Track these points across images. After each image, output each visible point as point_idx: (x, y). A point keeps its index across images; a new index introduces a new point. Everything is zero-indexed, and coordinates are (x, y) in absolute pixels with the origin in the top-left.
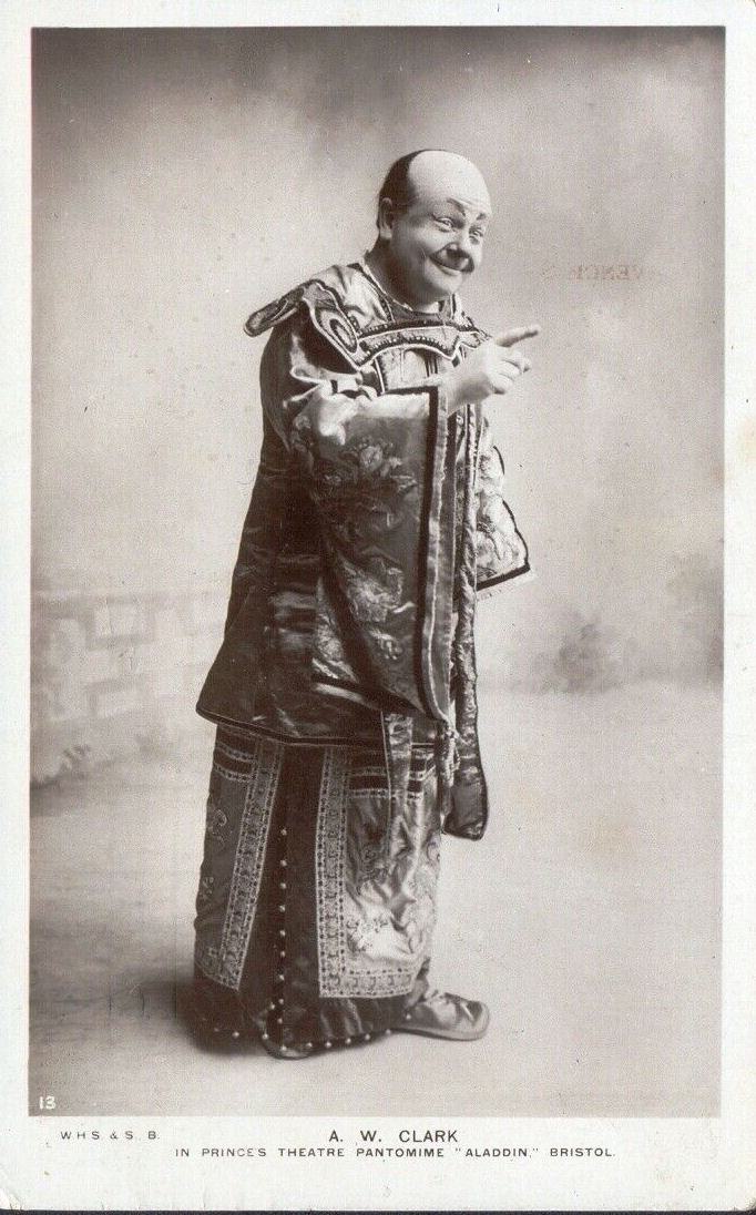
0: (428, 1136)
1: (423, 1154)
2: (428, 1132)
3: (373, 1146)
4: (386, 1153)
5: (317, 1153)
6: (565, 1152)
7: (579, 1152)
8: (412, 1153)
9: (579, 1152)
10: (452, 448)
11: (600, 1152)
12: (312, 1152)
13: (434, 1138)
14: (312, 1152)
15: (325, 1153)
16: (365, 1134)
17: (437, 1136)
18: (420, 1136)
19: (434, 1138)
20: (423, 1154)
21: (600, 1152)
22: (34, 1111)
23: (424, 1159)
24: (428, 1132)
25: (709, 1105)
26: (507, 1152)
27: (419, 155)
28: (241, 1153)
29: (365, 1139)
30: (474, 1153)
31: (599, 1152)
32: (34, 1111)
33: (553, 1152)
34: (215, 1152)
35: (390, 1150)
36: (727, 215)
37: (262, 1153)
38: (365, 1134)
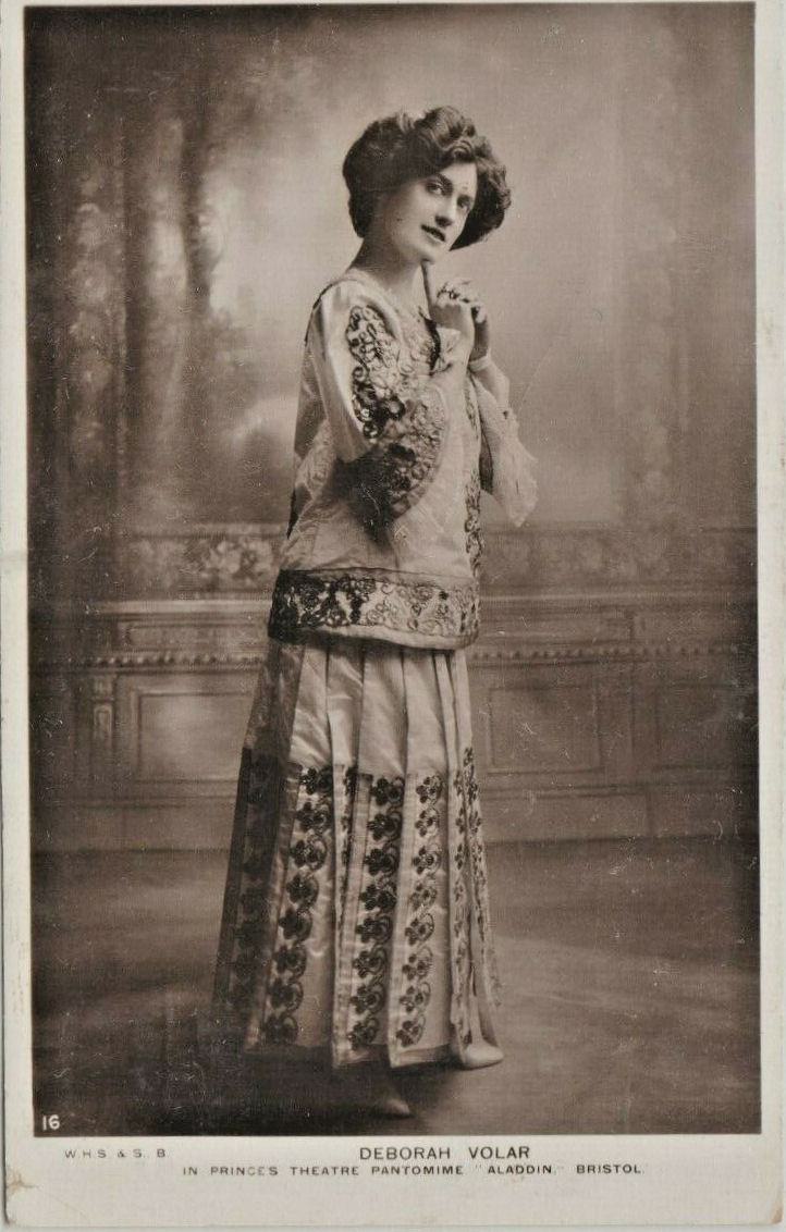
0: (512, 1152)
1: (597, 1167)
2: (512, 1149)
3: (523, 1161)
4: (402, 1170)
5: (331, 1171)
6: (591, 1168)
7: (607, 1169)
8: (429, 1170)
9: (607, 1169)
10: (476, 894)
11: (630, 1169)
12: (325, 1171)
13: (518, 1155)
14: (325, 1171)
15: (298, 1171)
16: (473, 1151)
17: (520, 1153)
18: (504, 1152)
19: (518, 1155)
20: (597, 1167)
21: (630, 1169)
22: (40, 1132)
23: (442, 1177)
24: (512, 1149)
25: (749, 1122)
26: (520, 1170)
27: (325, 662)
28: (251, 1172)
29: (474, 1156)
30: (496, 1170)
31: (416, 1170)
32: (40, 1132)
33: (580, 1169)
34: (224, 1170)
35: (617, 1167)
36: (358, 250)
37: (274, 1171)
38: (473, 1151)
